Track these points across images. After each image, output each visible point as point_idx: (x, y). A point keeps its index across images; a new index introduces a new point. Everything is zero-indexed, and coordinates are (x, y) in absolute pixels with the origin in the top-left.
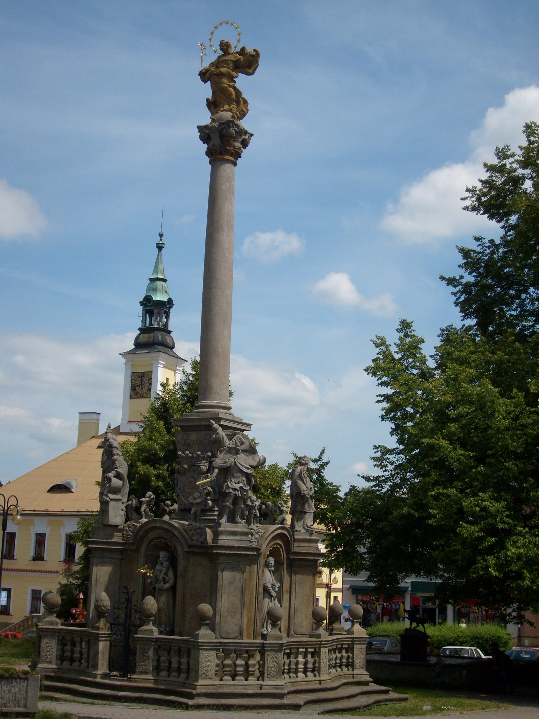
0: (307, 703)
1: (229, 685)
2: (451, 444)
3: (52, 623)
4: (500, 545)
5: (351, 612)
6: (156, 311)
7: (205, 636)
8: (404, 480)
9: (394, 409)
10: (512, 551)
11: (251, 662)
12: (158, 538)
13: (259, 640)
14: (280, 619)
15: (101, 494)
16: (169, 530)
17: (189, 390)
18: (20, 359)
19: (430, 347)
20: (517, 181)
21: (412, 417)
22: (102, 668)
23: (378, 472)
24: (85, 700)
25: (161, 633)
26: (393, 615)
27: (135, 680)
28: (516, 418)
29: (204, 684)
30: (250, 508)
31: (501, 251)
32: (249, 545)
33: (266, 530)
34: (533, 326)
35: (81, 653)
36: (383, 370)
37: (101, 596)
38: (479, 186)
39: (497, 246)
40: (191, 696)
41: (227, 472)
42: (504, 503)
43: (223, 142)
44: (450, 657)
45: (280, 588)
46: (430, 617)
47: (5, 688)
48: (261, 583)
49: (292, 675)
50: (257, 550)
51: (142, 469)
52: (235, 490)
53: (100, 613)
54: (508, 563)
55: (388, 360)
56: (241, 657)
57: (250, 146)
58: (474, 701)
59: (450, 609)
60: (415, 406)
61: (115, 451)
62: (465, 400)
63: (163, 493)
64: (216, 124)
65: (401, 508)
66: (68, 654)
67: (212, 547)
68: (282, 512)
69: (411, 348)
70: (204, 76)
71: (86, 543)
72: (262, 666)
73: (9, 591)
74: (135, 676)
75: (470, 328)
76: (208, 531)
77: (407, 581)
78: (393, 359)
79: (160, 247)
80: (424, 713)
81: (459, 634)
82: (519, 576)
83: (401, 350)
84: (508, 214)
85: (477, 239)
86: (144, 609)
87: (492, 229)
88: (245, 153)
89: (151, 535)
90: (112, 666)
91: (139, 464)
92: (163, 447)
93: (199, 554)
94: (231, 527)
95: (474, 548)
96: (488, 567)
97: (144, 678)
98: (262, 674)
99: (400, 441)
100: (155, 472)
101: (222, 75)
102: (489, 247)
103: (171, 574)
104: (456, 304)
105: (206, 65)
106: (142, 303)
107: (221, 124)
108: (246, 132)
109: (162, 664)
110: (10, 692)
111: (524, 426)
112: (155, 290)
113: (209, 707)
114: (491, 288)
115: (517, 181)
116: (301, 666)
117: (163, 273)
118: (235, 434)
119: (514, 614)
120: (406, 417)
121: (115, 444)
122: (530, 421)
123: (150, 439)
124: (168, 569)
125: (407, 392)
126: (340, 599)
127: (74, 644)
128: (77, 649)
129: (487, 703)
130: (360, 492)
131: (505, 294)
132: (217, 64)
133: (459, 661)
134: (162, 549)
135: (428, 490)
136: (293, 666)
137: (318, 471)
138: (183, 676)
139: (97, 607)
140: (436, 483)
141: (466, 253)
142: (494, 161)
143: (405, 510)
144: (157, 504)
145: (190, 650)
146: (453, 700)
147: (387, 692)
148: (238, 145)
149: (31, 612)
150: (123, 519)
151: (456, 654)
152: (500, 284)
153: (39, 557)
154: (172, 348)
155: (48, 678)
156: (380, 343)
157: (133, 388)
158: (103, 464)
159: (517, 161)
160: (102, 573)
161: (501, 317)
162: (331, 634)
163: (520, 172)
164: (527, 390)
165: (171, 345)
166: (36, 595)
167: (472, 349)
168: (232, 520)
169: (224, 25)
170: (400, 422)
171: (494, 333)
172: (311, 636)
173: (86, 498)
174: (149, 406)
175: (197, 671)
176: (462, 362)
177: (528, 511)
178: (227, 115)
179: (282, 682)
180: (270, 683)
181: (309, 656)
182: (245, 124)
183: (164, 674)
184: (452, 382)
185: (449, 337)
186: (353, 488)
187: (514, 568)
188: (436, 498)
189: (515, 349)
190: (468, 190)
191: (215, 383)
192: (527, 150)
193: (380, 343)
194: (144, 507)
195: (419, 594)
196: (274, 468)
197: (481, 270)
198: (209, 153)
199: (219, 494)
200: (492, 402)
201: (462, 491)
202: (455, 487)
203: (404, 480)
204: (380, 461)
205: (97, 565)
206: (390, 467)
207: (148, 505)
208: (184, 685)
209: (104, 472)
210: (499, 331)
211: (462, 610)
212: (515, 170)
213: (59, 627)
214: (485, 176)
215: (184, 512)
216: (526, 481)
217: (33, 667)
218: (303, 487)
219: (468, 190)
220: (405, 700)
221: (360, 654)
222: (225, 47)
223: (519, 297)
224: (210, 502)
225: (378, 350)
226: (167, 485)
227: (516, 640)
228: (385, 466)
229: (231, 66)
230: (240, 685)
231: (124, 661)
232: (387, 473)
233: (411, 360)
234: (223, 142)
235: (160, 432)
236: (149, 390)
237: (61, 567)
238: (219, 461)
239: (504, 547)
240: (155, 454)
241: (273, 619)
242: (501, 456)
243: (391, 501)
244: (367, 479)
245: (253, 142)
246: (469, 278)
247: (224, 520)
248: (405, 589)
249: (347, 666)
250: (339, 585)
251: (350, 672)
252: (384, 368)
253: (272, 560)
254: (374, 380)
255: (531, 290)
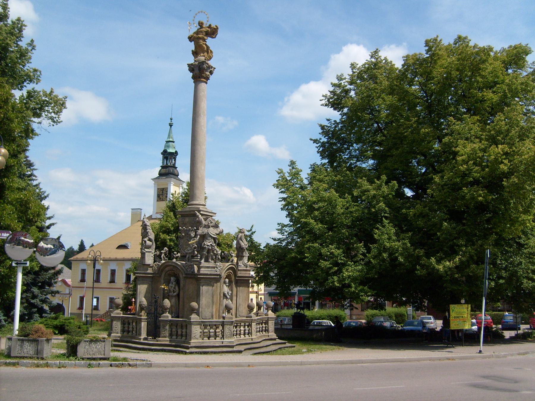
0: (245, 350)
1: (206, 342)
2: (315, 221)
3: (118, 314)
4: (340, 271)
5: (267, 305)
6: (169, 157)
7: (194, 318)
8: (293, 240)
9: (288, 205)
10: (346, 274)
11: (217, 330)
12: (170, 270)
13: (221, 320)
14: (232, 309)
15: (141, 249)
16: (175, 266)
17: (186, 196)
18: (101, 182)
19: (305, 175)
20: (347, 92)
21: (296, 209)
22: (144, 335)
23: (280, 236)
24: (135, 351)
25: (172, 317)
26: (288, 306)
27: (160, 341)
28: (347, 208)
29: (194, 342)
30: (216, 255)
31: (340, 126)
32: (216, 273)
33: (224, 266)
34: (356, 163)
35: (133, 328)
36: (282, 185)
37: (142, 299)
38: (329, 94)
39: (338, 124)
40: (188, 348)
41: (204, 237)
42: (341, 250)
43: (200, 72)
44: (317, 325)
45: (231, 294)
46: (308, 306)
47: (93, 346)
48: (222, 292)
49: (238, 336)
50: (220, 275)
51: (162, 236)
52: (208, 246)
53: (142, 308)
54: (344, 280)
55: (284, 180)
56: (213, 328)
57: (214, 74)
58: (328, 346)
59: (317, 303)
60: (297, 203)
61: (148, 228)
62: (322, 200)
63: (173, 248)
64: (197, 63)
65: (291, 253)
66: (126, 329)
67: (197, 275)
68: (232, 256)
69: (296, 174)
70: (191, 39)
71: (134, 274)
72: (223, 332)
73: (98, 299)
74: (160, 339)
75: (325, 164)
76: (195, 266)
77: (296, 290)
78: (287, 180)
79: (171, 125)
80: (303, 353)
81: (320, 315)
82: (349, 286)
83: (290, 175)
84: (343, 108)
85: (328, 120)
86: (164, 306)
87: (336, 115)
88: (211, 77)
89: (167, 269)
90: (148, 334)
91: (161, 234)
92: (173, 225)
93: (191, 278)
94: (206, 264)
95: (327, 273)
96: (334, 282)
97: (165, 340)
98: (223, 336)
99: (291, 221)
100: (169, 238)
101: (200, 38)
102: (334, 124)
103: (177, 288)
104: (318, 152)
105: (191, 33)
106: (162, 153)
107: (199, 63)
108: (212, 67)
109: (173, 333)
110: (96, 348)
111: (351, 212)
112: (168, 147)
113: (196, 353)
114: (335, 144)
115: (347, 92)
116: (242, 332)
117: (172, 138)
118: (208, 218)
119: (348, 305)
120: (293, 208)
121: (148, 224)
122: (354, 209)
123: (166, 221)
124: (175, 285)
125: (294, 196)
126: (263, 299)
127: (129, 324)
128: (131, 326)
129: (334, 347)
130: (271, 246)
131: (342, 147)
132: (197, 33)
133: (320, 327)
134: (172, 276)
135: (305, 244)
136: (238, 332)
137: (250, 236)
138: (184, 338)
139: (140, 305)
140: (308, 241)
141: (322, 127)
142: (336, 82)
143: (293, 255)
144: (170, 253)
145: (187, 325)
146: (318, 346)
147: (285, 343)
148: (208, 73)
149: (109, 309)
150: (153, 261)
151: (320, 324)
152: (339, 142)
153: (112, 281)
154: (178, 176)
155: (115, 340)
156: (280, 172)
157: (158, 196)
158: (142, 234)
159: (347, 81)
160: (142, 289)
161: (340, 159)
162: (257, 316)
163: (349, 87)
164: (353, 195)
165: (177, 174)
166: (112, 300)
167: (326, 174)
168: (207, 261)
169: (198, 14)
170: (290, 211)
171: (337, 166)
172: (247, 317)
173: (134, 252)
174: (165, 206)
175: (191, 335)
176: (320, 181)
177: (354, 254)
178: (202, 58)
179: (233, 340)
180: (227, 340)
181: (246, 327)
182: (210, 63)
183: (174, 337)
184: (316, 191)
185: (314, 169)
186: (268, 244)
187: (346, 282)
188: (309, 248)
189: (346, 174)
190: (323, 96)
191: (198, 192)
192: (352, 76)
193: (280, 172)
194: (163, 255)
195: (302, 296)
196: (228, 234)
197: (330, 135)
198: (193, 77)
199: (200, 248)
200: (335, 200)
201: (321, 245)
202: (318, 243)
203: (293, 240)
204: (281, 231)
205: (140, 284)
206: (286, 234)
207: (165, 255)
208: (184, 343)
209: (143, 238)
210: (339, 165)
211: (323, 303)
212: (346, 86)
213: (122, 315)
214: (332, 89)
215: (183, 257)
216: (352, 239)
217: (109, 335)
218: (242, 244)
219: (323, 96)
220: (294, 347)
221: (271, 326)
222: (201, 24)
223: (349, 149)
224: (196, 252)
225: (279, 175)
226: (175, 244)
227: (349, 317)
228: (283, 233)
229: (204, 34)
230: (212, 342)
231: (154, 331)
232: (284, 237)
233: (295, 180)
234: (200, 72)
235: (171, 218)
236: (167, 197)
237: (124, 286)
238: (200, 232)
239: (341, 272)
240: (169, 229)
241: (228, 309)
242: (340, 227)
243: (286, 250)
244: (275, 240)
245: (215, 72)
246: (324, 140)
247: (203, 261)
248: (294, 294)
249: (265, 331)
250: (262, 292)
251: (267, 334)
252: (283, 184)
253: (227, 280)
254: (277, 191)
255: (355, 145)
